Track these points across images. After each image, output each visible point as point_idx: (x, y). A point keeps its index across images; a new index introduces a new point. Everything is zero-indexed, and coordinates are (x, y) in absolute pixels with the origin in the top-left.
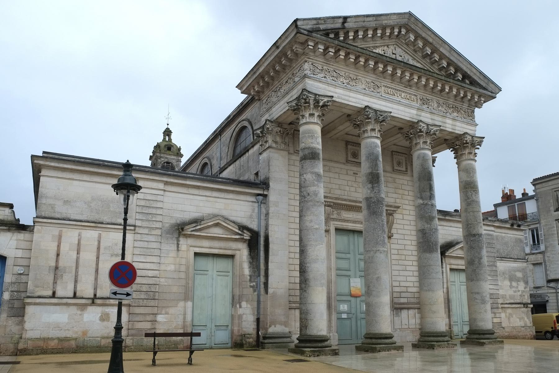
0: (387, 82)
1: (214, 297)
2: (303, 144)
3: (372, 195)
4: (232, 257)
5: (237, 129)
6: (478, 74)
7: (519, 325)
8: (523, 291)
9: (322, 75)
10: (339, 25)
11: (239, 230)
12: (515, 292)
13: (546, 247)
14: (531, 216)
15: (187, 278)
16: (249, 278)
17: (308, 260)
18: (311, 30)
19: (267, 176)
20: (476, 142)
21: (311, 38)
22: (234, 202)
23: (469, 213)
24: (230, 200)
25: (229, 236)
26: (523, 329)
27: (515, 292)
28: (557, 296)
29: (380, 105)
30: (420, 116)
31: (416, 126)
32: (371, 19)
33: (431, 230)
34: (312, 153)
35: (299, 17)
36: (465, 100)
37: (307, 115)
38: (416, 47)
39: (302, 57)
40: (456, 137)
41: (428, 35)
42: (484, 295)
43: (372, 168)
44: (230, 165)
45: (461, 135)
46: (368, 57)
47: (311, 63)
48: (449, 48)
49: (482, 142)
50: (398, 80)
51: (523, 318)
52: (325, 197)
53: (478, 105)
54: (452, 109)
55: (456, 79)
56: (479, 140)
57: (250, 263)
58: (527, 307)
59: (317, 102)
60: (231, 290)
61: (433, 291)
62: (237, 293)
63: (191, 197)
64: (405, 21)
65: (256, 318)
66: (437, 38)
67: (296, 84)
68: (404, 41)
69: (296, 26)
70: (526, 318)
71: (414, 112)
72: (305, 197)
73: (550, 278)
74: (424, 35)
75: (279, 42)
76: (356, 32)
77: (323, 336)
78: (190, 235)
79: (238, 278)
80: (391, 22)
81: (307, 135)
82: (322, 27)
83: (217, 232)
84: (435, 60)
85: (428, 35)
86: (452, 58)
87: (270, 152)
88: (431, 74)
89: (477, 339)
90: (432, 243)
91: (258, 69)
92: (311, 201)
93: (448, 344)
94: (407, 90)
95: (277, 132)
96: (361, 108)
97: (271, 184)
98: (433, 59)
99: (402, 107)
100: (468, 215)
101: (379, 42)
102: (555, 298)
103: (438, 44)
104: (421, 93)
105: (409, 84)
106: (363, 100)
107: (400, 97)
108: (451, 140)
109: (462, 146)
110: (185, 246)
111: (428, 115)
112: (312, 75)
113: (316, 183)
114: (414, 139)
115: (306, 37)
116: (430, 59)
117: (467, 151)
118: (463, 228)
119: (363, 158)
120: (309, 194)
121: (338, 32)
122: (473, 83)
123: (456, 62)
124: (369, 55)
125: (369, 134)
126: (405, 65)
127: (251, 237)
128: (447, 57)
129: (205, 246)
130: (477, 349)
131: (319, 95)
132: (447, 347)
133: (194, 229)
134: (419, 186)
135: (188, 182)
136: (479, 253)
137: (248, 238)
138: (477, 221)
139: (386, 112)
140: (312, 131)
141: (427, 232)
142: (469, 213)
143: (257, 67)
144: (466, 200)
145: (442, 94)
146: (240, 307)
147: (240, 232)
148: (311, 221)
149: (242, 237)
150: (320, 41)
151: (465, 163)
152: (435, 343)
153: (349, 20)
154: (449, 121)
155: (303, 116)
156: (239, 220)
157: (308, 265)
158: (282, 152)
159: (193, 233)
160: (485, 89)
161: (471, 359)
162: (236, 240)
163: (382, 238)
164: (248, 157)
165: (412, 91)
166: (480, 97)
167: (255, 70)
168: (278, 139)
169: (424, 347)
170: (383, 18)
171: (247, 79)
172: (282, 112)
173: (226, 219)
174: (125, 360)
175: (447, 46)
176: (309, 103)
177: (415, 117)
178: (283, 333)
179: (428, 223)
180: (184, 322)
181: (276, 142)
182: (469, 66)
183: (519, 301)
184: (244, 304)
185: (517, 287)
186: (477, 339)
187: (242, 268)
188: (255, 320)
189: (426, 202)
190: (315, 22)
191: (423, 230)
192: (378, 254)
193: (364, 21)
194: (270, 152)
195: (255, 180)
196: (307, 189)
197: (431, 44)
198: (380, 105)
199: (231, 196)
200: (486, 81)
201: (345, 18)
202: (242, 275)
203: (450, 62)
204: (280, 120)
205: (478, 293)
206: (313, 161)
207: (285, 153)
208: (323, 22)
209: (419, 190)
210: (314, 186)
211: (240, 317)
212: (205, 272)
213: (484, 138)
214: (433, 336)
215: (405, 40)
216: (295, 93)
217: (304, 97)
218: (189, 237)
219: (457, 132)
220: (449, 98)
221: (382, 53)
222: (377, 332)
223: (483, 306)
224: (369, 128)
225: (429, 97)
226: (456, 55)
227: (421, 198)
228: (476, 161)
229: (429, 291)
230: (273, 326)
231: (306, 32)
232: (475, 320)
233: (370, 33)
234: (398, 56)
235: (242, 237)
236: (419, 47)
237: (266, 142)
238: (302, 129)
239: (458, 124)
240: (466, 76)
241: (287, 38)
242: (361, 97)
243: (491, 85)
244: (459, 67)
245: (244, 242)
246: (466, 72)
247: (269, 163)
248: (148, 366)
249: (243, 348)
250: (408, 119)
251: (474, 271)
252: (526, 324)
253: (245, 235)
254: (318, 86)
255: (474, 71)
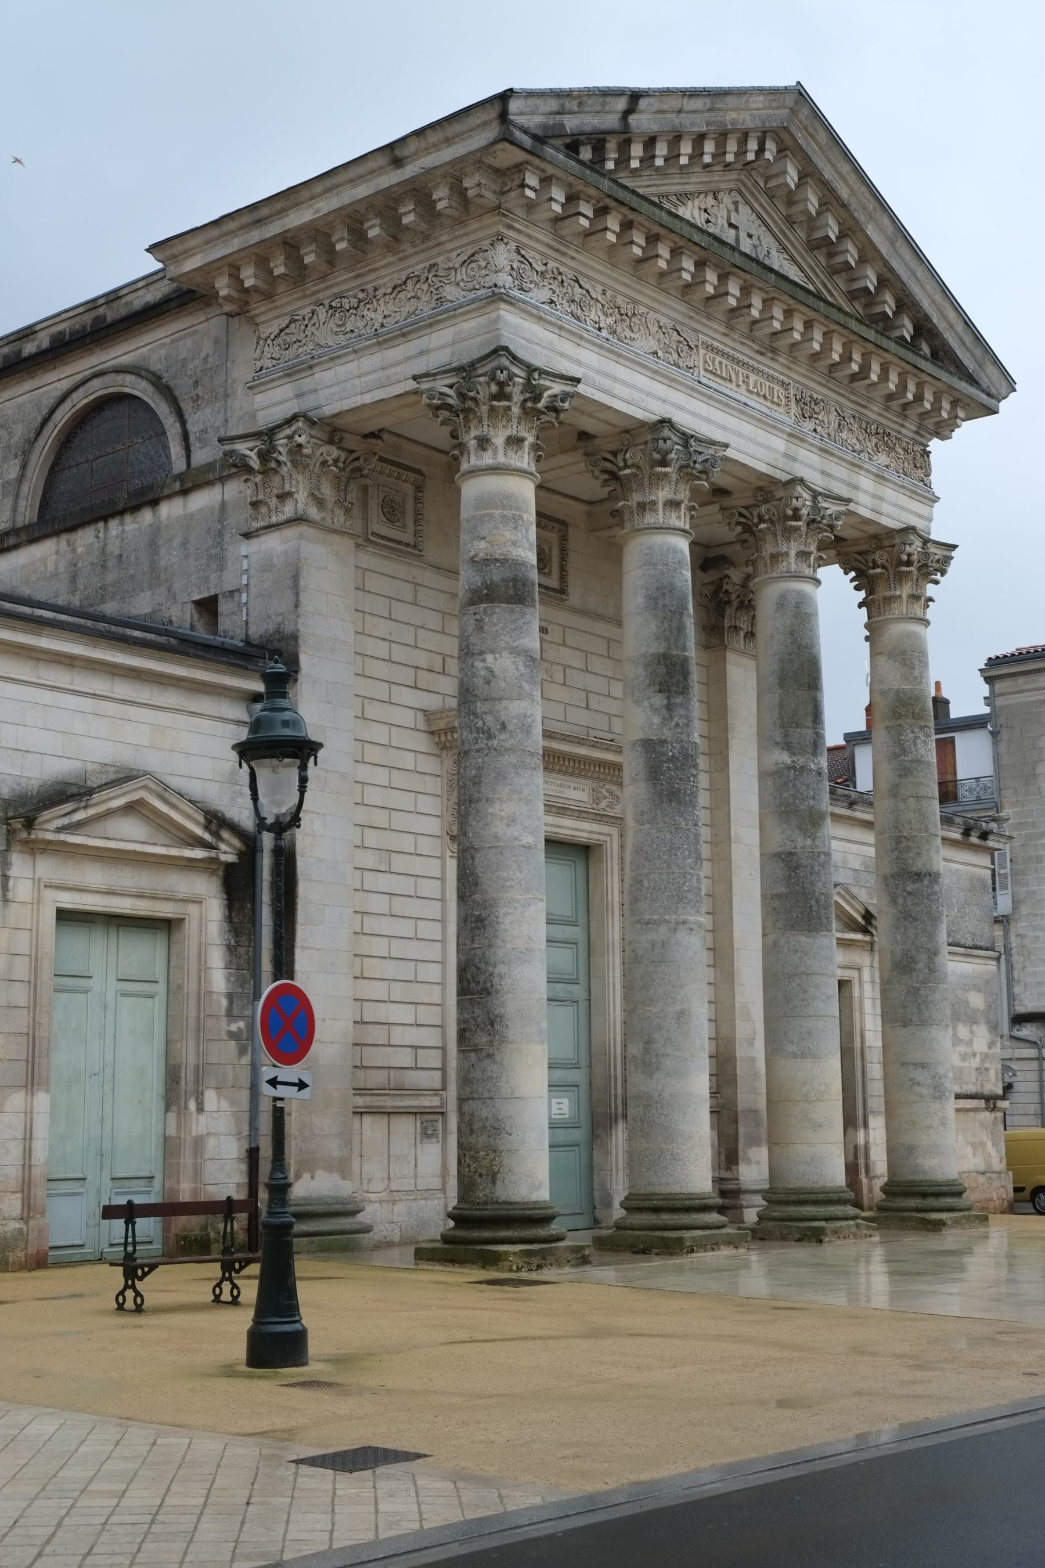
0: (711, 332)
1: (109, 1071)
2: (483, 544)
3: (667, 734)
4: (167, 926)
5: (80, 400)
6: (960, 327)
7: (972, 1167)
8: (985, 1057)
9: (545, 294)
10: (611, 121)
11: (207, 828)
12: (964, 1057)
13: (1016, 903)
14: (970, 790)
15: (34, 1006)
16: (224, 1002)
17: (501, 953)
18: (540, 133)
19: (288, 628)
20: (935, 560)
21: (537, 161)
22: (181, 719)
23: (904, 801)
24: (170, 715)
25: (174, 852)
26: (982, 1179)
27: (964, 1057)
28: (1041, 1066)
29: (694, 414)
30: (794, 459)
31: (779, 494)
32: (698, 104)
33: (814, 855)
34: (514, 580)
35: (516, 86)
36: (914, 412)
37: (499, 440)
38: (795, 209)
39: (489, 219)
40: (875, 537)
41: (840, 174)
42: (941, 1070)
43: (667, 639)
44: (33, 541)
45: (891, 532)
46: (682, 243)
47: (513, 245)
48: (890, 229)
49: (948, 560)
50: (745, 329)
51: (982, 1144)
52: (548, 735)
53: (943, 430)
54: (874, 440)
55: (896, 333)
56: (940, 553)
57: (231, 949)
58: (994, 1109)
59: (534, 393)
60: (162, 1047)
61: (816, 1057)
62: (188, 1055)
63: (48, 696)
64: (778, 116)
65: (246, 1146)
66: (864, 189)
67: (445, 313)
68: (761, 183)
69: (503, 116)
70: (989, 1144)
71: (779, 444)
72: (490, 736)
73: (1021, 1009)
74: (828, 173)
75: (412, 146)
76: (650, 142)
77: (537, 1205)
78: (49, 842)
79: (193, 1004)
80: (745, 119)
81: (497, 513)
82: (571, 123)
83: (130, 834)
84: (847, 263)
85: (840, 174)
86: (895, 264)
87: (301, 537)
88: (841, 318)
89: (917, 1210)
90: (817, 901)
91: (282, 212)
92: (511, 750)
93: (858, 1226)
94: (764, 363)
95: (324, 463)
96: (643, 424)
97: (303, 659)
98: (839, 259)
99: (748, 428)
100: (902, 806)
101: (696, 181)
102: (1034, 1076)
103: (865, 208)
104: (800, 377)
105: (770, 347)
106: (648, 394)
107: (744, 387)
108: (856, 541)
109: (892, 566)
110: (29, 883)
111: (814, 458)
112: (517, 293)
113: (527, 686)
114: (769, 538)
115: (522, 156)
116: (830, 255)
117: (905, 590)
118: (878, 845)
119: (634, 600)
120: (503, 726)
121: (604, 141)
122: (942, 354)
123: (905, 276)
124: (666, 230)
125: (659, 517)
126: (780, 281)
127: (240, 854)
128: (882, 258)
129: (95, 888)
130: (913, 1242)
131: (542, 372)
132: (855, 1236)
133: (66, 821)
134: (782, 706)
135: (47, 642)
136: (931, 936)
137: (230, 858)
138: (927, 831)
139: (713, 443)
140: (504, 495)
141: (804, 862)
142: (904, 801)
143: (278, 206)
144: (896, 756)
145: (855, 385)
146: (200, 1109)
147: (207, 837)
148: (512, 820)
149: (213, 854)
150: (559, 173)
151: (897, 629)
152: (822, 1224)
153: (643, 103)
154: (866, 483)
155: (484, 443)
156: (196, 789)
157: (500, 969)
158: (337, 538)
159: (62, 837)
160: (972, 380)
161: (891, 1273)
162: (191, 865)
163: (694, 881)
164: (156, 531)
165: (775, 368)
166: (954, 403)
167: (265, 212)
168: (327, 490)
169: (783, 1238)
170: (731, 101)
171: (215, 232)
172: (367, 399)
173: (165, 791)
174: (302, 1279)
175: (886, 221)
176: (508, 397)
177: (782, 462)
178: (339, 1201)
179: (805, 832)
180: (27, 1166)
181: (320, 503)
182: (939, 298)
183: (972, 1089)
184: (210, 1098)
185: (970, 1043)
186: (917, 1210)
187: (203, 969)
188: (244, 1155)
189: (801, 760)
190: (553, 105)
191: (790, 854)
192: (682, 935)
193: (680, 112)
194: (301, 537)
195: (192, 628)
196: (499, 706)
197: (844, 206)
198: (694, 414)
199: (171, 698)
200: (978, 352)
201: (635, 96)
202: (204, 995)
203: (888, 275)
204: (340, 422)
205: (923, 1066)
206: (518, 608)
207: (345, 544)
208: (573, 105)
209: (781, 718)
210: (520, 697)
211: (199, 1143)
212: (82, 982)
213: (955, 547)
214: (815, 1203)
215: (767, 179)
216: (446, 345)
217: (502, 376)
218: (43, 851)
219: (885, 521)
220: (870, 399)
221: (699, 220)
222: (676, 1189)
223: (935, 1106)
224: (662, 495)
225: (820, 392)
226: (908, 256)
227: (787, 746)
228: (927, 623)
229: (803, 1055)
230: (306, 1176)
231: (527, 141)
232: (911, 1150)
233: (686, 148)
234: (743, 235)
235: (213, 854)
236: (807, 212)
237: (283, 496)
238: (471, 490)
239: (889, 493)
240: (924, 329)
241: (448, 141)
242: (642, 380)
243: (991, 369)
244: (910, 295)
245: (213, 872)
246: (927, 318)
247: (296, 578)
248: (105, 1313)
249: (208, 1252)
250: (763, 468)
251: (914, 992)
252: (988, 1164)
253: (223, 847)
254: (535, 337)
255: (952, 315)
